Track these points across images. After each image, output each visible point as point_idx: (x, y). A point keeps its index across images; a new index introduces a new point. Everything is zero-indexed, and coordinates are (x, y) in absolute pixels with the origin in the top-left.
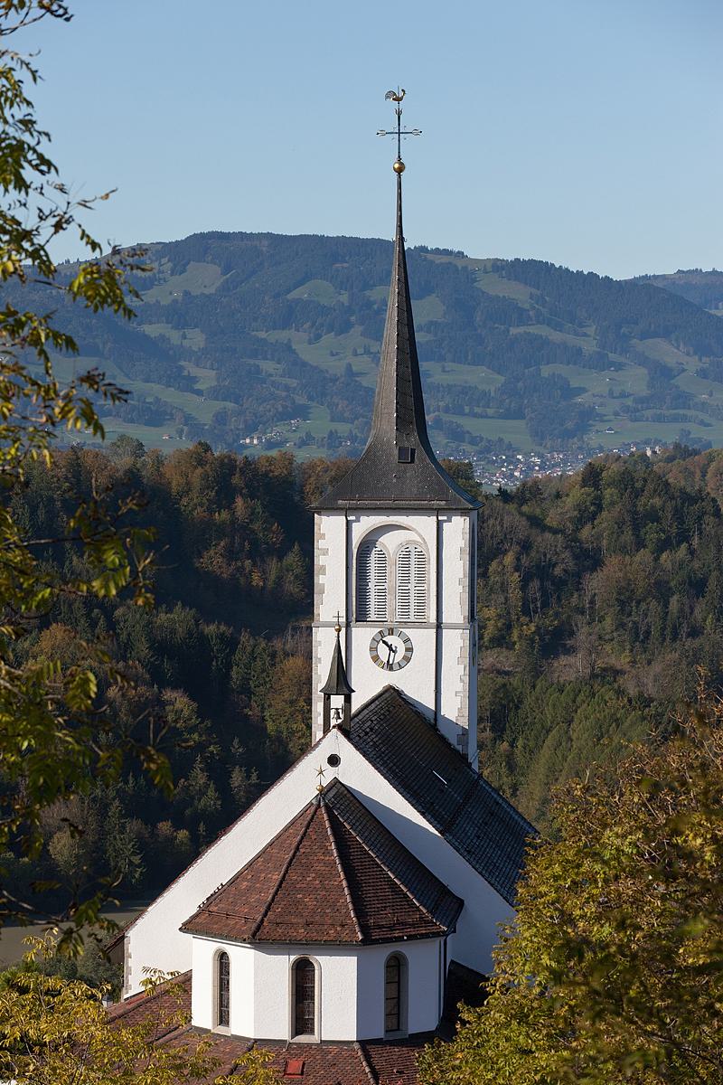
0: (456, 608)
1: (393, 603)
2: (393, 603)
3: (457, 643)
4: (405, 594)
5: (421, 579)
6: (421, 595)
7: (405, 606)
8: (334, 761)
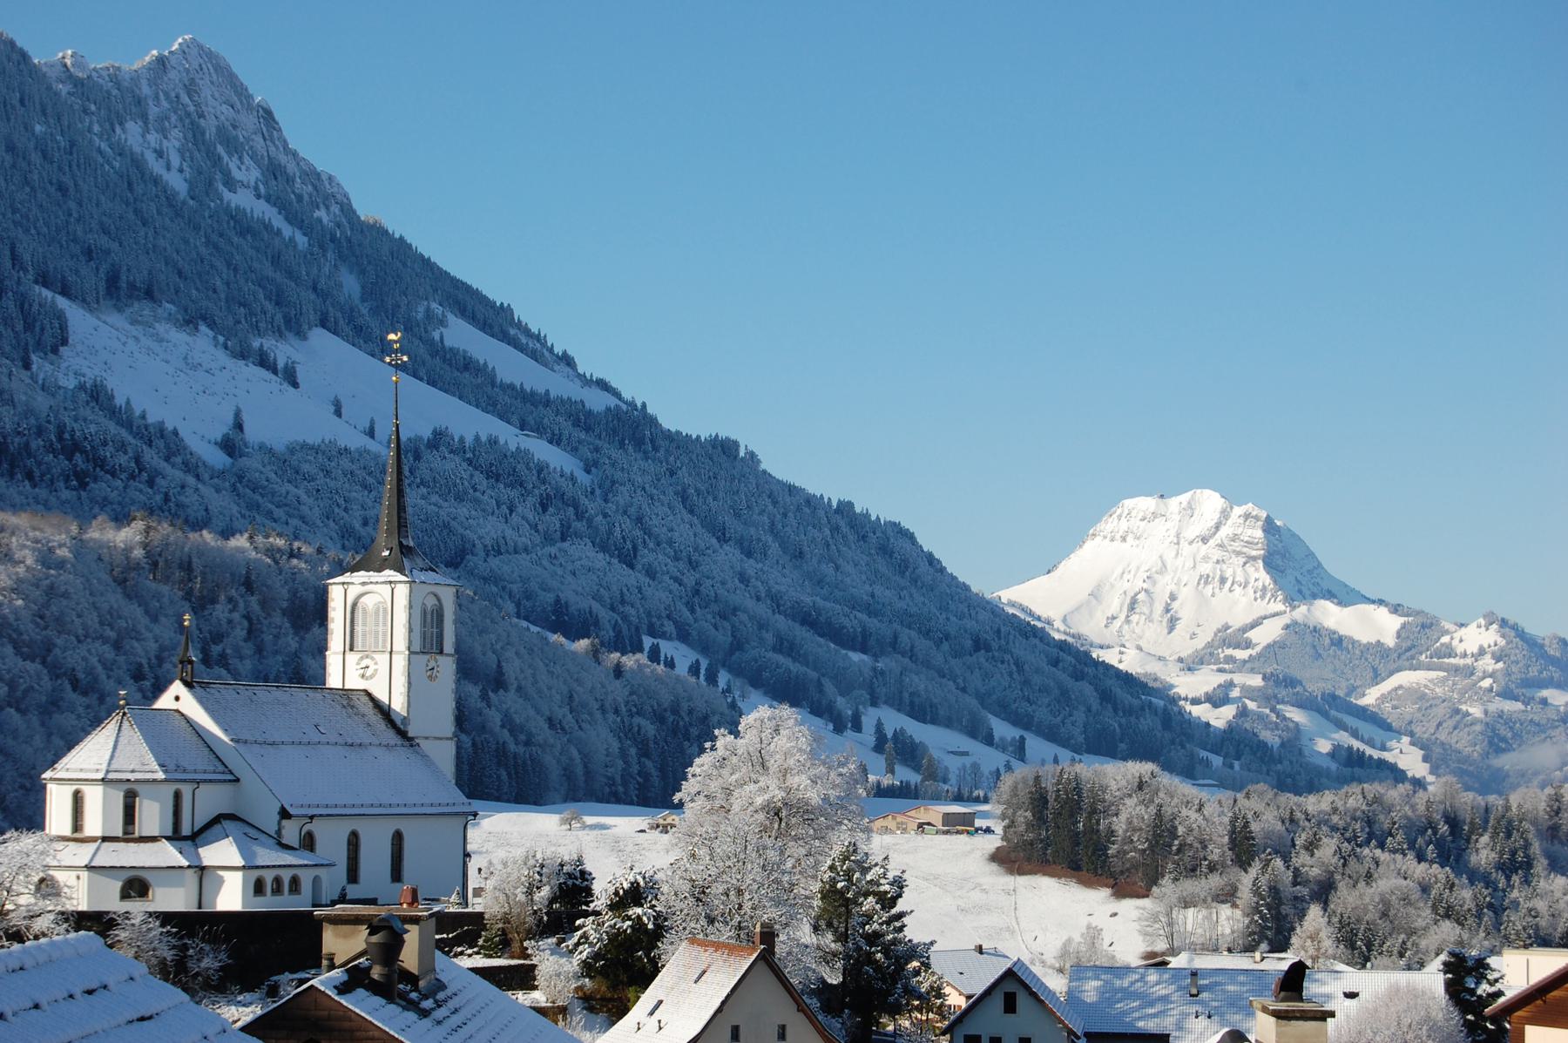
0: (401, 643)
1: (370, 640)
2: (370, 640)
3: (400, 662)
4: (377, 632)
5: (385, 624)
6: (385, 634)
7: (376, 638)
8: (177, 698)
